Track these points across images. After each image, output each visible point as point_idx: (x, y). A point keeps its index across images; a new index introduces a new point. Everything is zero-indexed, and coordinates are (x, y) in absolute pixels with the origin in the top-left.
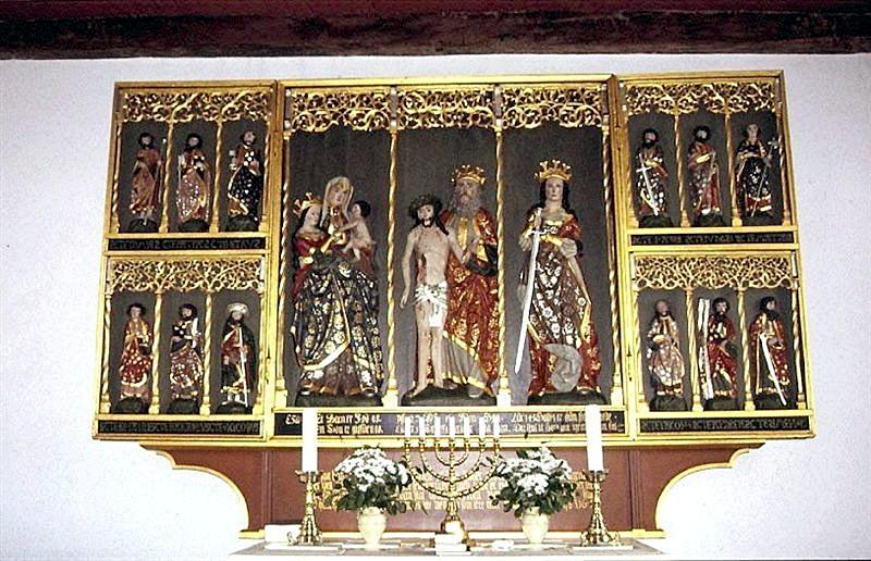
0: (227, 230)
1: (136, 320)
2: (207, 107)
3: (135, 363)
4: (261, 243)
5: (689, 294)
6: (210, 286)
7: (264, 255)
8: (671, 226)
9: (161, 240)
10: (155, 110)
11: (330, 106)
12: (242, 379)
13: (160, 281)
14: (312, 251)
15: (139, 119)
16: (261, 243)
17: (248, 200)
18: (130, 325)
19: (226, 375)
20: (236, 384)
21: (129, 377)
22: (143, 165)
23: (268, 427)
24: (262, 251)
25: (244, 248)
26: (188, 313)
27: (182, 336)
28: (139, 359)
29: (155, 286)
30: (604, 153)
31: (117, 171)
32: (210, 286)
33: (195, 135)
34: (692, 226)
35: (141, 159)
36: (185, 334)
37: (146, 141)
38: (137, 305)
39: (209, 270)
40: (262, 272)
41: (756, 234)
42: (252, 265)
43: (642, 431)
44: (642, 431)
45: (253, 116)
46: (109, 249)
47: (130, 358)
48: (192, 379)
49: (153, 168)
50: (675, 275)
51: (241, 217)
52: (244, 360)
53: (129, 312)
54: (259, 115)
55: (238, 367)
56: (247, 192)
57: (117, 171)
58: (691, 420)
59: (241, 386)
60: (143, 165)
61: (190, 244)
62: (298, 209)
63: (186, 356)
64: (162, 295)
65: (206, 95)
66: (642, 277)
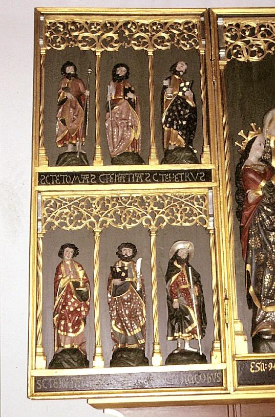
0: (58, 164)
1: (68, 263)
2: (136, 36)
3: (72, 309)
4: (207, 176)
5: (97, 234)
6: (153, 223)
7: (210, 188)
8: (82, 164)
9: (152, 172)
10: (80, 38)
11: (263, 36)
12: (196, 323)
13: (97, 218)
14: (263, 184)
15: (63, 47)
16: (207, 176)
17: (185, 132)
18: (63, 268)
19: (177, 319)
20: (190, 328)
21: (66, 326)
22: (69, 96)
23: (231, 378)
24: (208, 184)
25: (188, 181)
26: (128, 252)
27: (123, 279)
28: (76, 305)
29: (148, 221)
30: (202, 83)
31: (43, 101)
32: (153, 223)
33: (122, 65)
34: (161, 163)
35: (66, 89)
36: (126, 276)
37: (70, 70)
38: (72, 246)
39: (151, 206)
40: (210, 207)
41: (72, 174)
42: (197, 200)
43: (239, 384)
44: (239, 384)
45: (184, 45)
46: (211, 181)
47: (67, 304)
48: (138, 325)
49: (80, 97)
50: (195, 212)
51: (179, 149)
52: (195, 303)
53: (61, 254)
54: (191, 45)
55: (190, 310)
56: (184, 123)
57: (43, 101)
58: (149, 377)
59: (193, 332)
60: (69, 96)
61: (128, 178)
62: (241, 140)
63: (130, 300)
64: (156, 232)
65: (133, 23)
66: (49, 219)
